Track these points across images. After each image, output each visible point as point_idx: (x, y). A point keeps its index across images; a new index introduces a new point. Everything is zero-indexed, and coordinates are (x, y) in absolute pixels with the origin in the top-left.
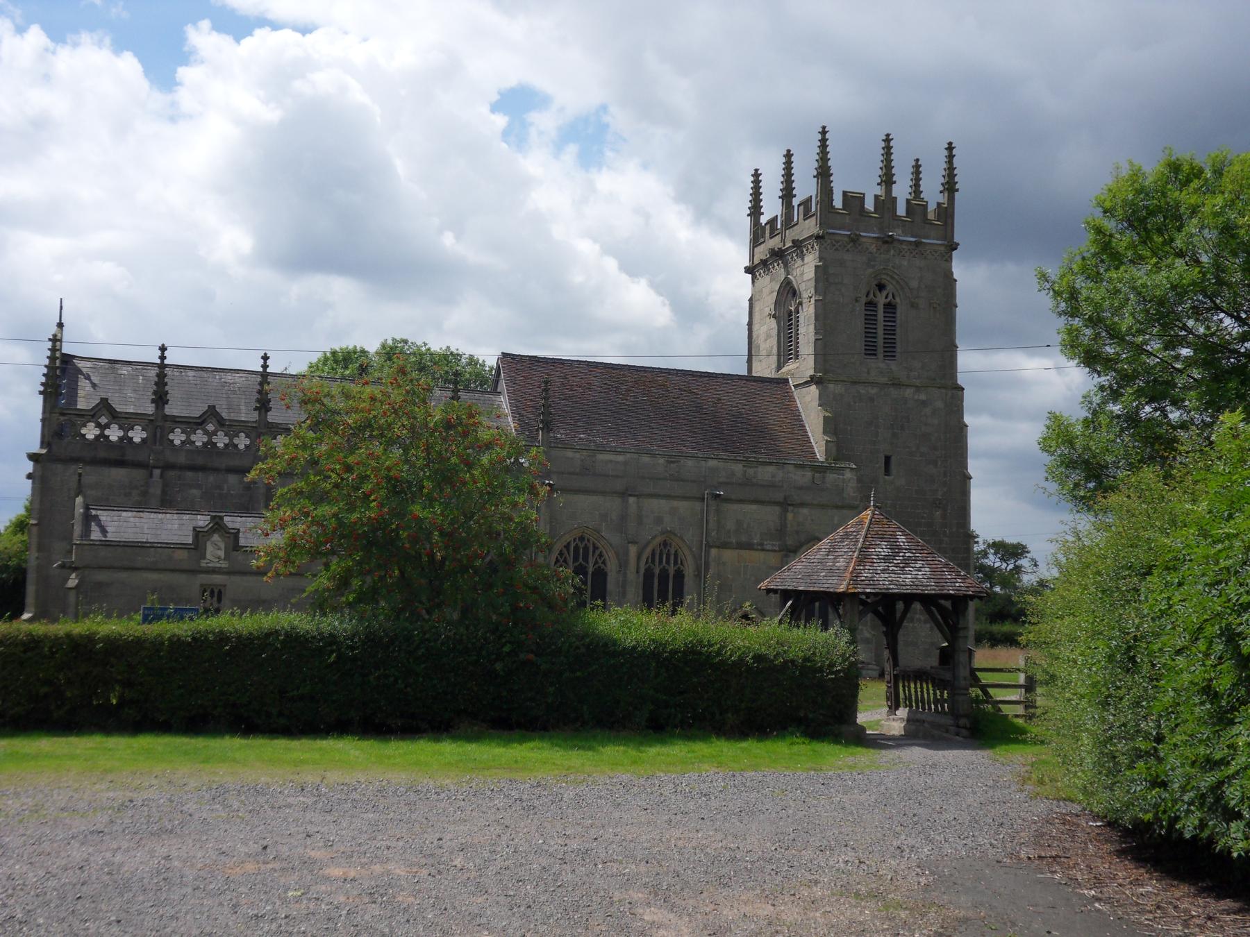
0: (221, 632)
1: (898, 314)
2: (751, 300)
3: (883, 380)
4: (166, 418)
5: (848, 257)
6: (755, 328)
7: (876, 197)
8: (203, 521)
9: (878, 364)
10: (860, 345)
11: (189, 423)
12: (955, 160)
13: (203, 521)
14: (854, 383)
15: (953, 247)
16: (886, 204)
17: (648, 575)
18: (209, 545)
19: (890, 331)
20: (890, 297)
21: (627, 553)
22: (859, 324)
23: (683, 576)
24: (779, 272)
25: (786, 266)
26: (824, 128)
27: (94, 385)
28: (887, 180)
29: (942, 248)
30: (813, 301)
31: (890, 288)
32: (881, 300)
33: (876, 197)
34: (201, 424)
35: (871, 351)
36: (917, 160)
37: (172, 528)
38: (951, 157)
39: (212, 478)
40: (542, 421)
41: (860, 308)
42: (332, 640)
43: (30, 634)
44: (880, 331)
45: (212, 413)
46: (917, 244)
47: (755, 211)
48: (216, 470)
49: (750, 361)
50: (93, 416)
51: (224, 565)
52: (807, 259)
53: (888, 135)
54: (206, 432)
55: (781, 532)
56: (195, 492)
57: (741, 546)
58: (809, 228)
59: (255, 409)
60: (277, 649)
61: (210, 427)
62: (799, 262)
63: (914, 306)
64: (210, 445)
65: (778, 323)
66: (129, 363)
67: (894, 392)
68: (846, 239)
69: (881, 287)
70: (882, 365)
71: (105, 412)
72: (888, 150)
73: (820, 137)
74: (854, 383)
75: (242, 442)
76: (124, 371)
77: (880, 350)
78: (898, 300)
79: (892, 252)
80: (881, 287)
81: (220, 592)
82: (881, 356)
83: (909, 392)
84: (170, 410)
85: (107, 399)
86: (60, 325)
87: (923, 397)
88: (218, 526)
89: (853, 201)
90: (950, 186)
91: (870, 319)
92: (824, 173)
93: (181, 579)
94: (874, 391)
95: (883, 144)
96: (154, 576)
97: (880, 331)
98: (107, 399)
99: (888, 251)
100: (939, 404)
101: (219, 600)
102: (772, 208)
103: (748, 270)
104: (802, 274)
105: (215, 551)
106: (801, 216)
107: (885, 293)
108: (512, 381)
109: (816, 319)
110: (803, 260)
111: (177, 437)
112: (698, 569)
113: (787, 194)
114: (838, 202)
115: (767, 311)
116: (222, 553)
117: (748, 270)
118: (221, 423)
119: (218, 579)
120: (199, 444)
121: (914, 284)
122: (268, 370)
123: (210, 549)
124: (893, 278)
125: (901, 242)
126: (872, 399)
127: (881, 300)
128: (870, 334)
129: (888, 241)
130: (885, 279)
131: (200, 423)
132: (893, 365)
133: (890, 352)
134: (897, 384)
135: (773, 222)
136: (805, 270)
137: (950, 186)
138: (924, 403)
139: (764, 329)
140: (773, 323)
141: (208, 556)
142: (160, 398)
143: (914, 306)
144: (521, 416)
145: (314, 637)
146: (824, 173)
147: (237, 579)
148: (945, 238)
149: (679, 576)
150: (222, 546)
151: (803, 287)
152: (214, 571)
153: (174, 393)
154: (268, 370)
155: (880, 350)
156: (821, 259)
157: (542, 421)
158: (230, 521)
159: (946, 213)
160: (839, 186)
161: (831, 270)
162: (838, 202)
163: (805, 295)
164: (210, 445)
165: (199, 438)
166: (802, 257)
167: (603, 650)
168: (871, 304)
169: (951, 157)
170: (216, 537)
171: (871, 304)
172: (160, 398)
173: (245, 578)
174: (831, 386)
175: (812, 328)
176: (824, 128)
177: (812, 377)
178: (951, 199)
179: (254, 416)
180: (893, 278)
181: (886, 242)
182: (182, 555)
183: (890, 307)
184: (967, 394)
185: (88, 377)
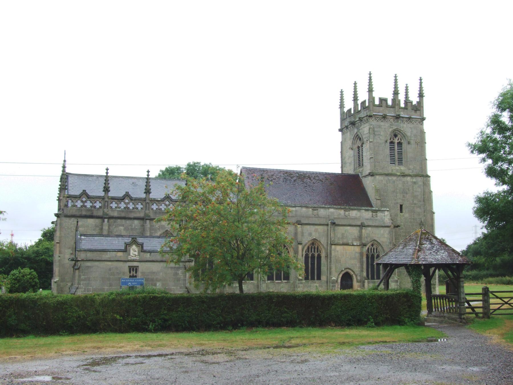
1: (403, 147)
2: (342, 143)
5: (382, 124)
16: (395, 100)
18: (131, 249)
19: (400, 153)
20: (399, 140)
21: (298, 248)
22: (388, 151)
28: (396, 93)
31: (399, 136)
32: (396, 141)
34: (123, 199)
36: (407, 85)
38: (421, 83)
39: (128, 222)
44: (396, 154)
45: (127, 195)
46: (410, 118)
47: (342, 106)
48: (130, 219)
51: (137, 258)
54: (125, 203)
55: (360, 237)
56: (122, 228)
57: (343, 244)
61: (127, 201)
64: (127, 208)
69: (396, 136)
70: (397, 168)
81: (136, 269)
82: (397, 163)
86: (65, 161)
89: (383, 101)
90: (421, 95)
91: (392, 149)
92: (370, 90)
96: (110, 263)
99: (398, 121)
101: (136, 272)
102: (349, 105)
103: (341, 130)
107: (397, 138)
112: (327, 254)
113: (355, 99)
114: (377, 102)
116: (136, 253)
117: (341, 130)
119: (135, 264)
121: (409, 134)
122: (109, 175)
123: (132, 251)
127: (396, 141)
128: (392, 156)
131: (122, 199)
132: (402, 168)
137: (421, 95)
141: (131, 254)
146: (370, 90)
147: (142, 263)
149: (319, 257)
150: (137, 250)
154: (109, 175)
159: (418, 108)
163: (365, 140)
164: (127, 208)
165: (123, 205)
168: (392, 143)
169: (421, 83)
170: (134, 247)
172: (106, 190)
174: (377, 177)
176: (421, 78)
183: (400, 144)
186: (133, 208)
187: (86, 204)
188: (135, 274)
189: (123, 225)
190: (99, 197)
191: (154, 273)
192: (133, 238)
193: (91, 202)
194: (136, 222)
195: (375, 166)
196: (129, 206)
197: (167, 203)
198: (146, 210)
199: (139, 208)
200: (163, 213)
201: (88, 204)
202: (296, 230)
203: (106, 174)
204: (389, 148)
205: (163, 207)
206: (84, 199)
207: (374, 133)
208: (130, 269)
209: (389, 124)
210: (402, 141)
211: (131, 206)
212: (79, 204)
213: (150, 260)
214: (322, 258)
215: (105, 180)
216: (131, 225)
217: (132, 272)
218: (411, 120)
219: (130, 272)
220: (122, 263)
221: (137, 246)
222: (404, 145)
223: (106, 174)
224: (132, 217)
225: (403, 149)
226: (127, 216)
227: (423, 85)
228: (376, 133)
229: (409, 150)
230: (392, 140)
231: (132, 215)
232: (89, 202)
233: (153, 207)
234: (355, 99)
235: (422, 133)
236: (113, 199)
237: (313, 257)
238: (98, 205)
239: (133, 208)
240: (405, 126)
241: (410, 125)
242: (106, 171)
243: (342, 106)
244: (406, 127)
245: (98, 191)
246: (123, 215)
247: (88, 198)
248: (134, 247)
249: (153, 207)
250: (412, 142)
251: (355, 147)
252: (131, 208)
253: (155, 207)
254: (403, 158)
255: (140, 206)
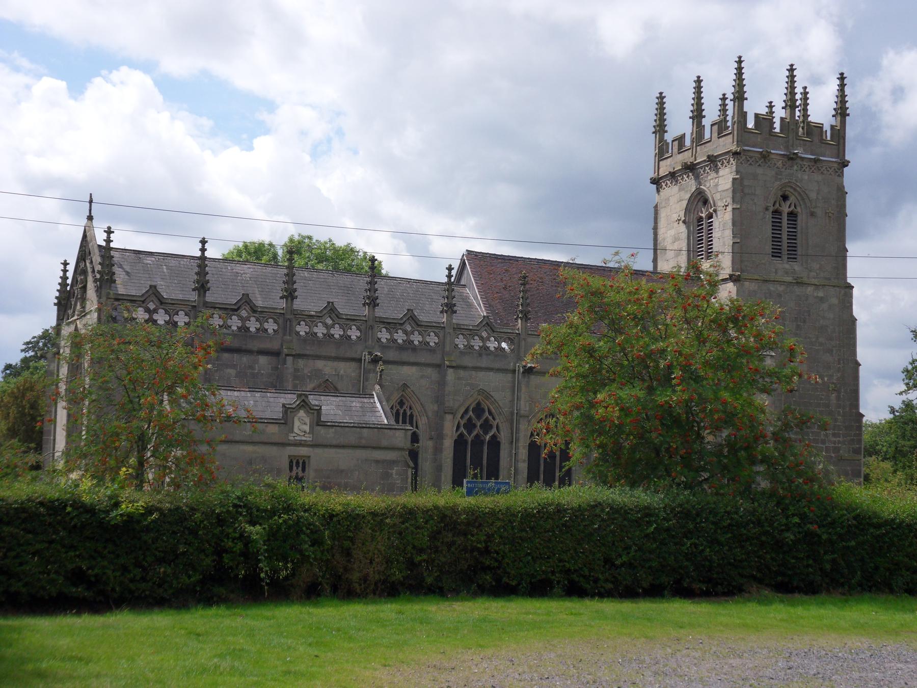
0: (558, 504)
1: (799, 222)
3: (789, 279)
4: (207, 305)
5: (760, 171)
6: (661, 231)
7: (782, 119)
8: (290, 399)
9: (783, 265)
10: (768, 249)
11: (226, 309)
12: (846, 88)
13: (290, 399)
14: (766, 281)
15: (845, 164)
17: (460, 443)
18: (296, 420)
19: (792, 236)
20: (793, 207)
22: (768, 230)
23: (498, 443)
24: (689, 184)
25: (697, 177)
26: (740, 57)
27: (128, 273)
29: (836, 165)
30: (729, 209)
31: (792, 199)
32: (785, 209)
33: (782, 119)
34: (236, 310)
35: (776, 254)
37: (269, 404)
39: (245, 359)
40: (521, 312)
41: (769, 215)
42: (647, 512)
43: (404, 507)
44: (785, 236)
45: (246, 300)
46: (816, 161)
47: (660, 127)
48: (249, 352)
49: (655, 261)
50: (143, 302)
51: (308, 438)
52: (721, 172)
53: (792, 65)
54: (241, 318)
56: (232, 372)
58: (727, 144)
59: (194, 290)
60: (603, 520)
61: (244, 313)
62: (713, 174)
63: (812, 214)
64: (244, 329)
65: (688, 228)
66: (151, 254)
67: (798, 290)
68: (758, 155)
69: (785, 198)
70: (787, 266)
71: (154, 298)
72: (791, 78)
73: (736, 65)
74: (766, 281)
75: (271, 326)
76: (149, 260)
77: (785, 252)
78: (799, 209)
79: (795, 167)
80: (785, 198)
81: (304, 463)
82: (785, 257)
83: (810, 289)
84: (298, 304)
85: (155, 287)
87: (821, 294)
88: (304, 404)
91: (776, 226)
93: (273, 451)
94: (781, 288)
95: (787, 73)
96: (250, 448)
97: (785, 236)
98: (155, 287)
99: (792, 166)
100: (834, 301)
101: (304, 470)
102: (680, 123)
104: (717, 185)
105: (301, 425)
106: (715, 135)
107: (788, 203)
108: (478, 275)
109: (734, 224)
110: (717, 172)
111: (302, 329)
113: (698, 114)
114: (751, 124)
115: (675, 217)
116: (307, 428)
118: (161, 301)
119: (303, 451)
120: (234, 328)
121: (813, 195)
122: (112, 245)
123: (297, 423)
124: (795, 190)
125: (803, 159)
126: (780, 296)
127: (785, 209)
128: (776, 239)
129: (792, 158)
130: (789, 191)
131: (232, 310)
132: (796, 267)
133: (793, 253)
134: (799, 283)
135: (681, 139)
136: (721, 183)
137: (842, 111)
138: (822, 299)
139: (672, 233)
140: (683, 228)
141: (296, 430)
142: (202, 287)
143: (812, 214)
144: (490, 306)
145: (632, 510)
147: (319, 451)
148: (838, 157)
149: (495, 444)
150: (307, 420)
151: (717, 196)
152: (300, 444)
153: (120, 276)
154: (112, 245)
155: (785, 252)
156: (737, 172)
157: (521, 312)
158: (313, 400)
159: (839, 134)
160: (754, 106)
161: (746, 183)
162: (751, 124)
163: (720, 204)
164: (244, 329)
165: (235, 323)
166: (717, 170)
167: (863, 523)
168: (777, 212)
169: (842, 86)
170: (302, 413)
171: (777, 212)
172: (202, 287)
173: (326, 450)
174: (747, 284)
175: (728, 233)
176: (740, 57)
177: (731, 276)
178: (843, 123)
179: (193, 297)
180: (795, 190)
181: (792, 159)
182: (273, 429)
183: (792, 215)
184: (855, 292)
185: (121, 266)
186: (258, 330)
187: (155, 317)
188: (300, 474)
189: (234, 366)
190: (182, 303)
191: (342, 471)
192: (299, 396)
193: (167, 312)
194: (263, 360)
195: (742, 261)
196: (248, 324)
197: (329, 321)
198: (284, 334)
199: (270, 331)
200: (320, 342)
201: (337, 332)
202: (442, 383)
203: (199, 254)
204: (771, 224)
205: (400, 337)
206: (152, 306)
207: (742, 191)
208: (291, 462)
209: (773, 173)
210: (799, 209)
211: (253, 326)
212: (235, 323)
213: (334, 442)
214: (502, 447)
215: (199, 266)
216: (251, 367)
217: (295, 468)
218: (819, 165)
219: (291, 469)
220: (333, 450)
221: (307, 412)
222: (802, 219)
223: (199, 254)
224: (255, 349)
225: (799, 228)
226: (244, 347)
227: (847, 90)
228: (746, 191)
229: (811, 230)
230: (793, 207)
231: (255, 345)
232: (161, 311)
233: (298, 328)
234: (698, 114)
235: (841, 194)
236: (213, 306)
237: (478, 441)
238: (354, 334)
239: (258, 330)
240: (806, 177)
241: (817, 177)
242: (200, 246)
243: (660, 127)
244: (810, 183)
245: (178, 290)
246: (236, 344)
247: (162, 303)
248: (302, 413)
249: (298, 328)
250: (819, 212)
251: (693, 217)
252: (253, 329)
253: (302, 329)
254: (799, 245)
255: (271, 326)
